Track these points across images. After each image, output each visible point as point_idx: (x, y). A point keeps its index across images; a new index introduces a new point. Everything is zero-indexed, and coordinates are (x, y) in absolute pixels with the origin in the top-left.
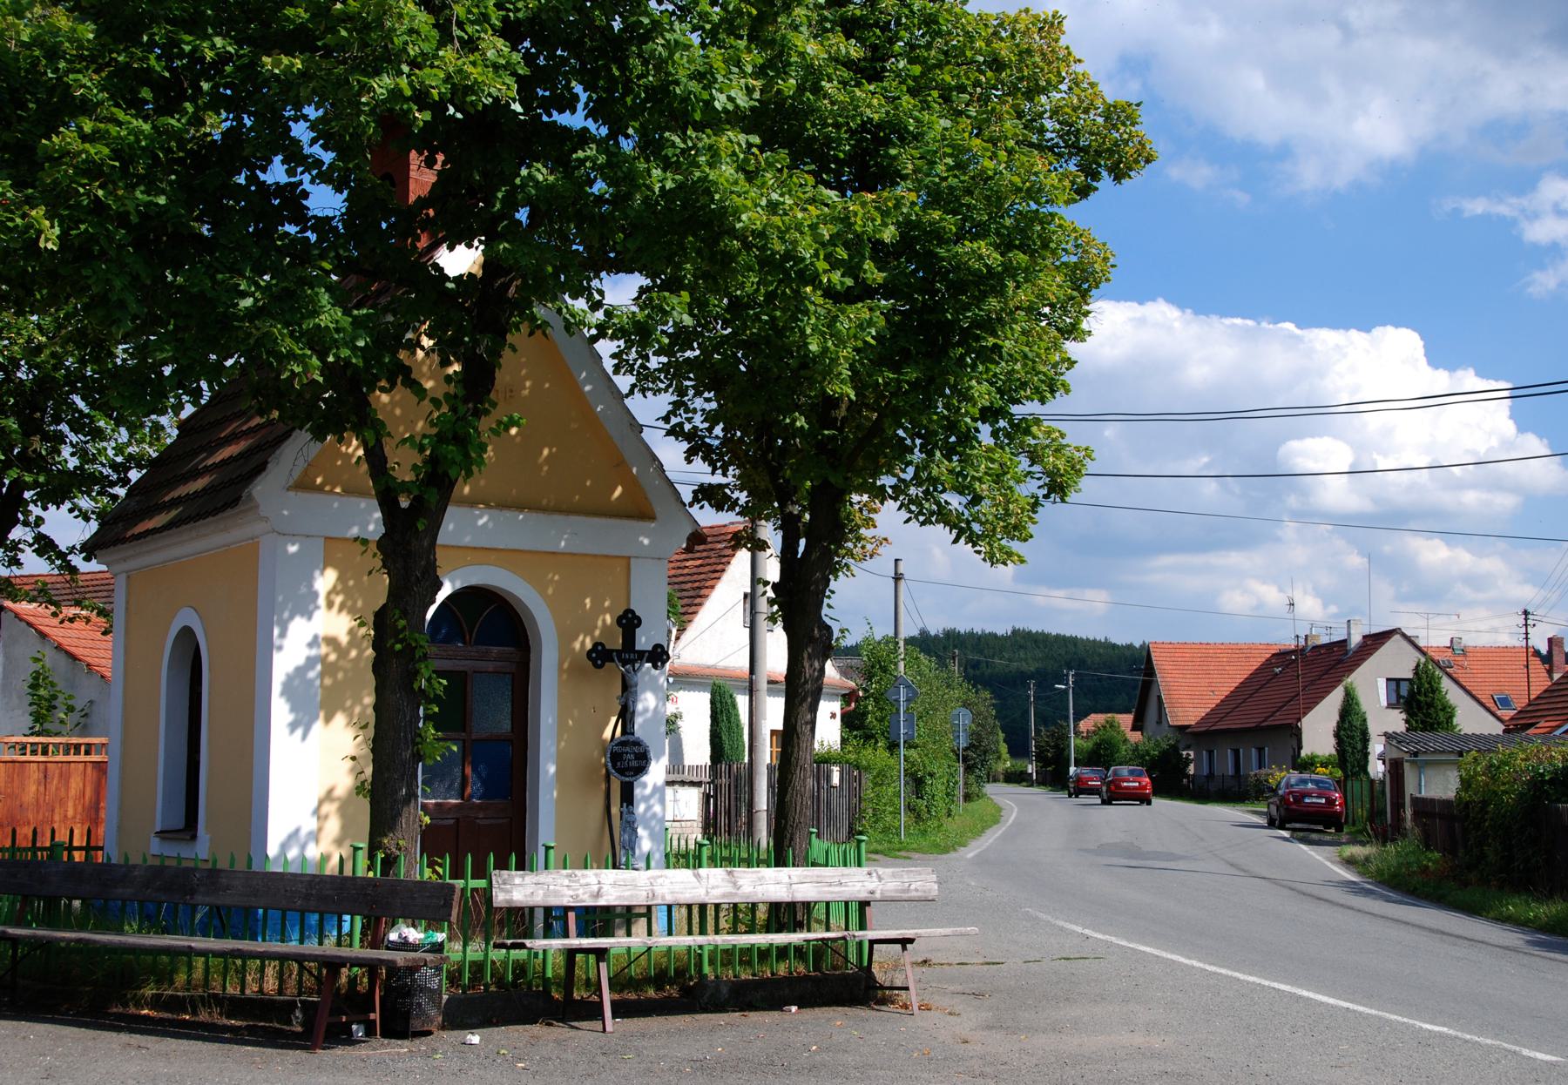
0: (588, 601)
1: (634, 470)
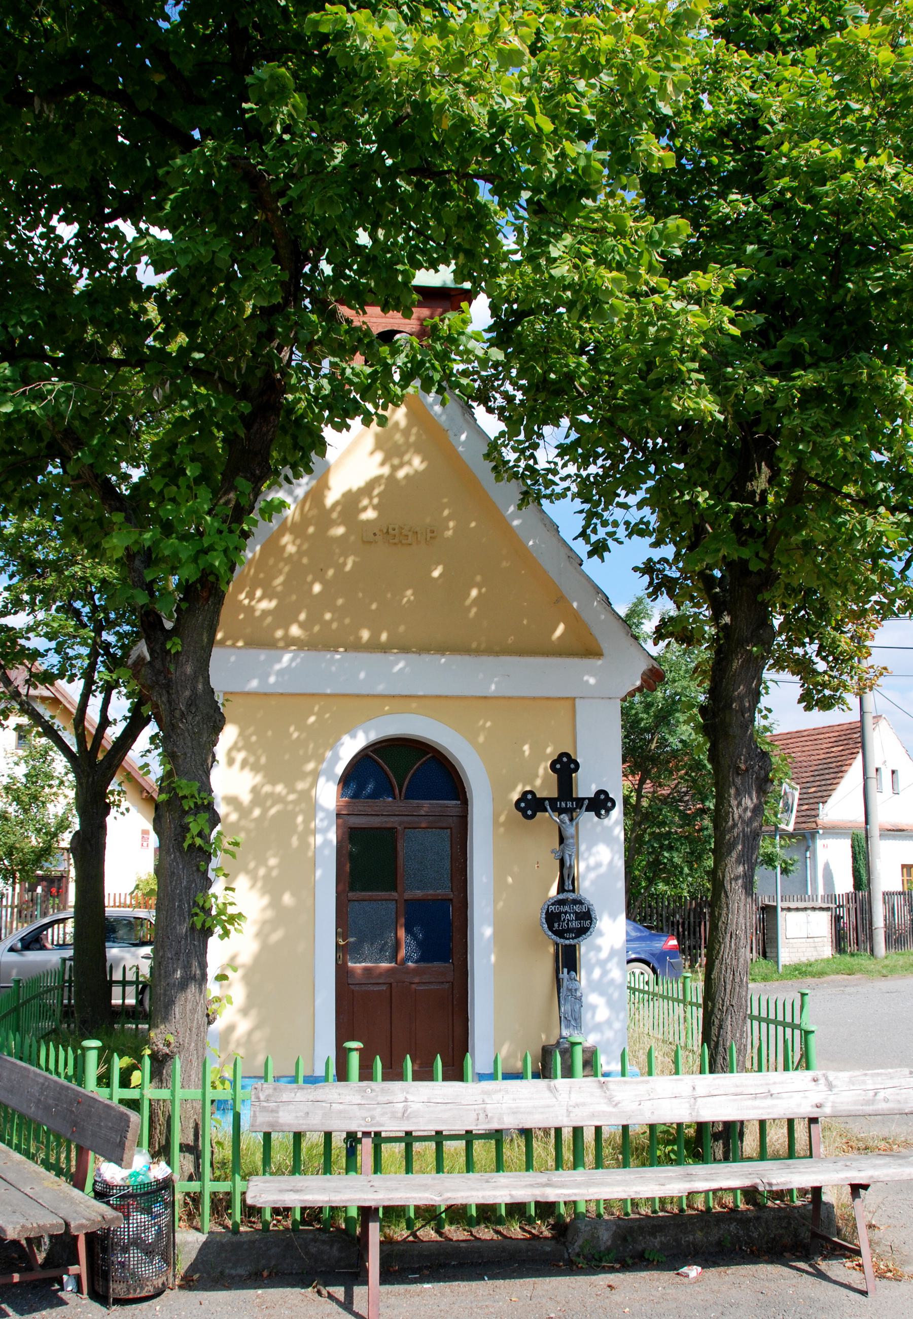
0: (526, 748)
1: (575, 605)
